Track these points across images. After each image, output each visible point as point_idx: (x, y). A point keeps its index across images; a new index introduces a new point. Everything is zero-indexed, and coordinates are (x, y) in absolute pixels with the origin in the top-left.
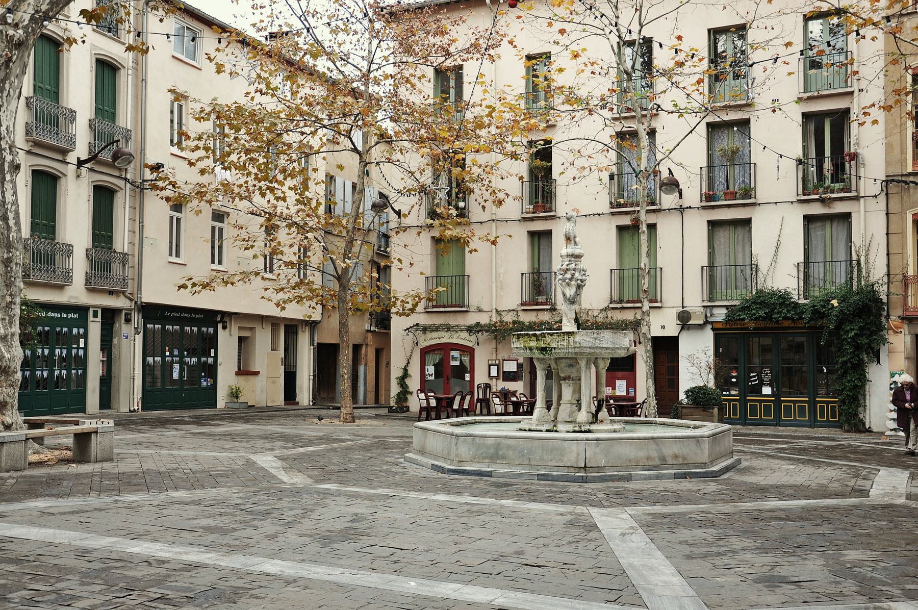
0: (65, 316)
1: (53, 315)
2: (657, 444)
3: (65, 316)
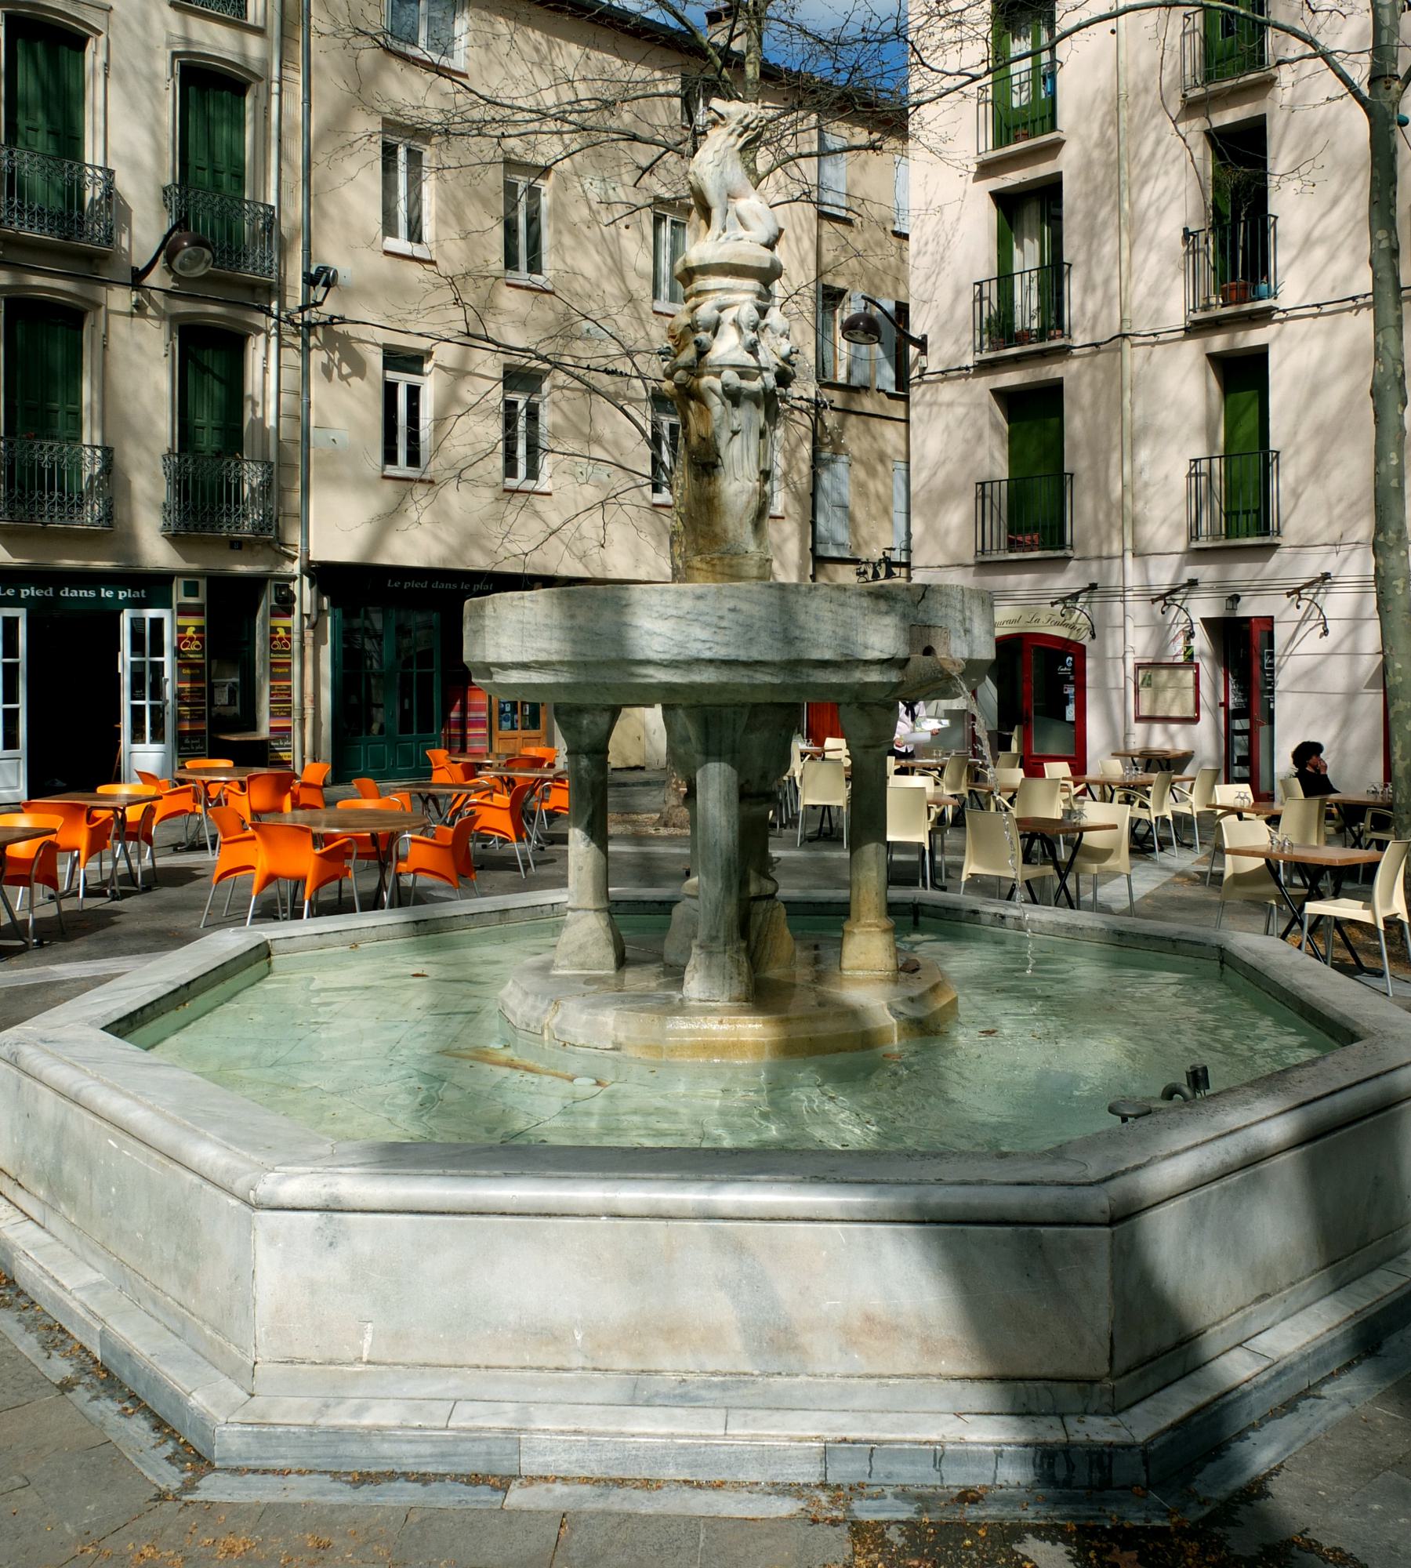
0: (109, 594)
1: (74, 594)
2: (739, 1248)
3: (109, 594)
